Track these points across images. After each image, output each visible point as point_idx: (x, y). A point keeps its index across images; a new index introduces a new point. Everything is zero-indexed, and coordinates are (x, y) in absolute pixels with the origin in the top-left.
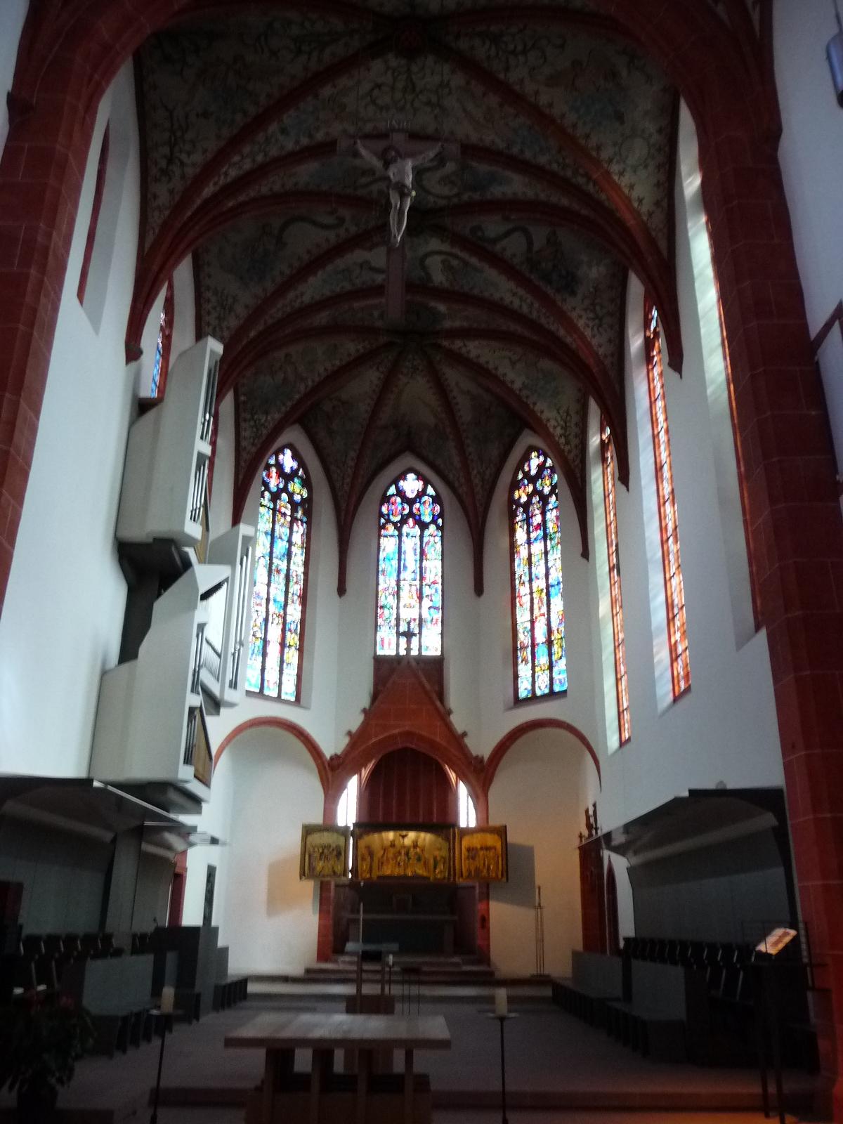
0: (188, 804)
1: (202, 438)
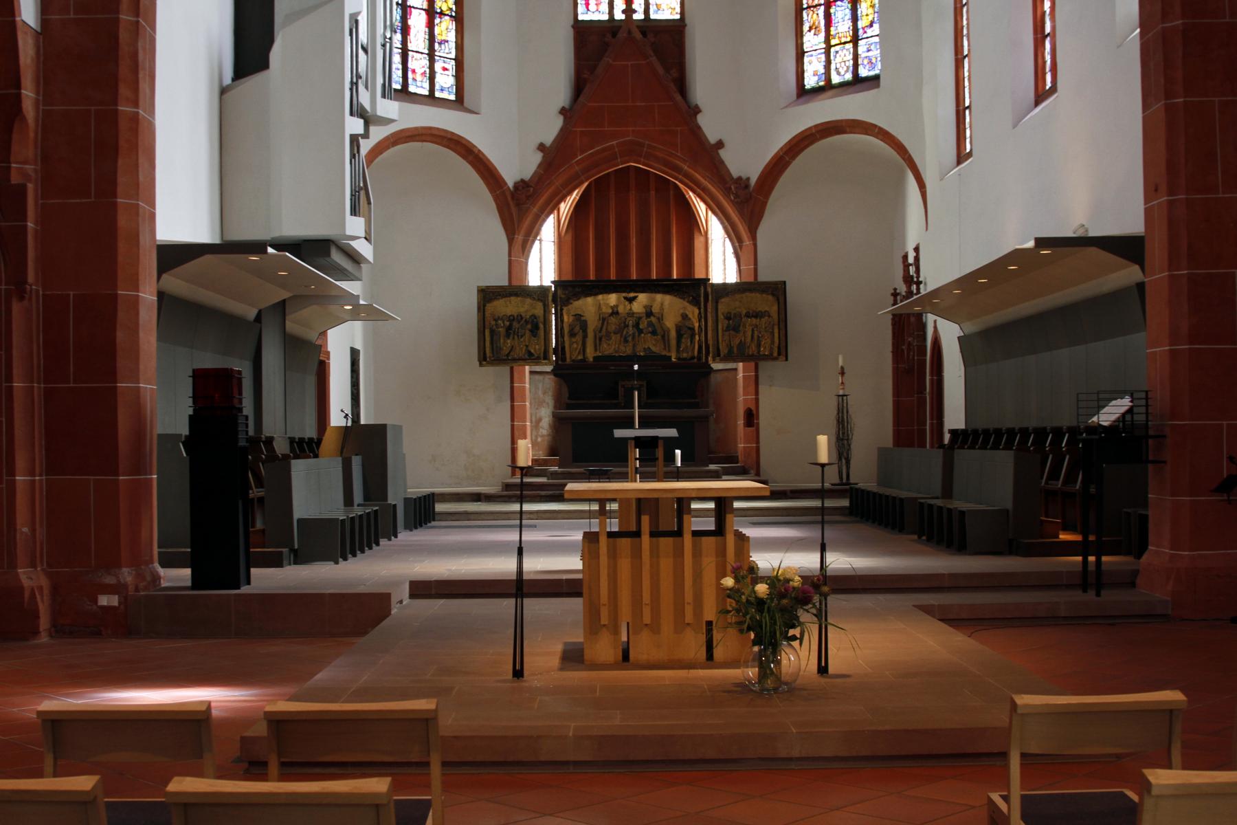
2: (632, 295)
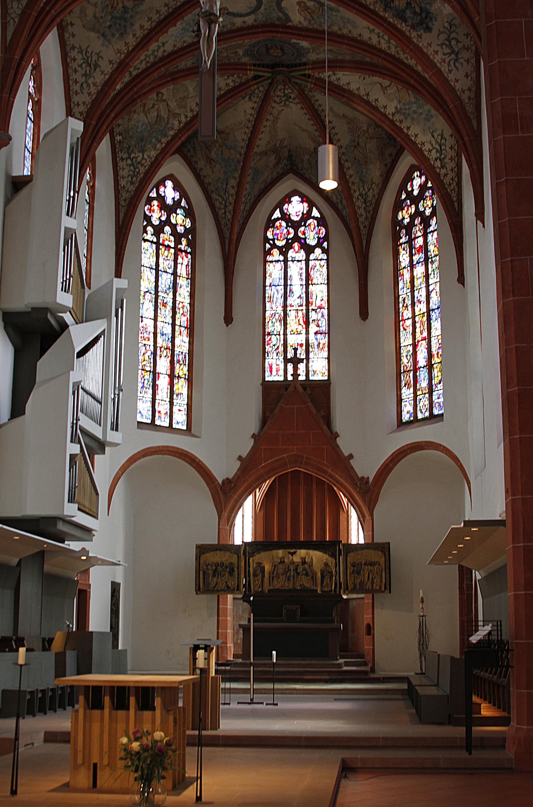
0: (78, 533)
1: (68, 215)
2: (293, 551)
